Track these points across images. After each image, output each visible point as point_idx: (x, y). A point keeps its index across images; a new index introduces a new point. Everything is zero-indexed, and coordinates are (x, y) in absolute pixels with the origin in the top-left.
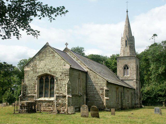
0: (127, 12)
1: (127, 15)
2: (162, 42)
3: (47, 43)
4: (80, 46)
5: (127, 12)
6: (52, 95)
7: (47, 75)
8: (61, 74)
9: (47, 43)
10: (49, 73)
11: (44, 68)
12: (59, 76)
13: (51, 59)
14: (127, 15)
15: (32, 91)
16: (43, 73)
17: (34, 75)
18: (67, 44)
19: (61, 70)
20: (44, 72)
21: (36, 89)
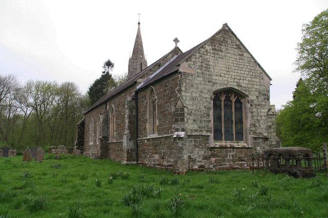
0: (139, 24)
1: (139, 30)
2: (297, 86)
3: (226, 25)
4: (107, 60)
5: (139, 24)
6: (240, 136)
7: (229, 91)
8: (257, 94)
9: (226, 25)
10: (236, 88)
11: (227, 76)
12: (255, 97)
13: (238, 60)
14: (139, 30)
15: (204, 124)
16: (225, 86)
17: (205, 86)
18: (176, 41)
19: (258, 87)
20: (226, 85)
21: (210, 121)
